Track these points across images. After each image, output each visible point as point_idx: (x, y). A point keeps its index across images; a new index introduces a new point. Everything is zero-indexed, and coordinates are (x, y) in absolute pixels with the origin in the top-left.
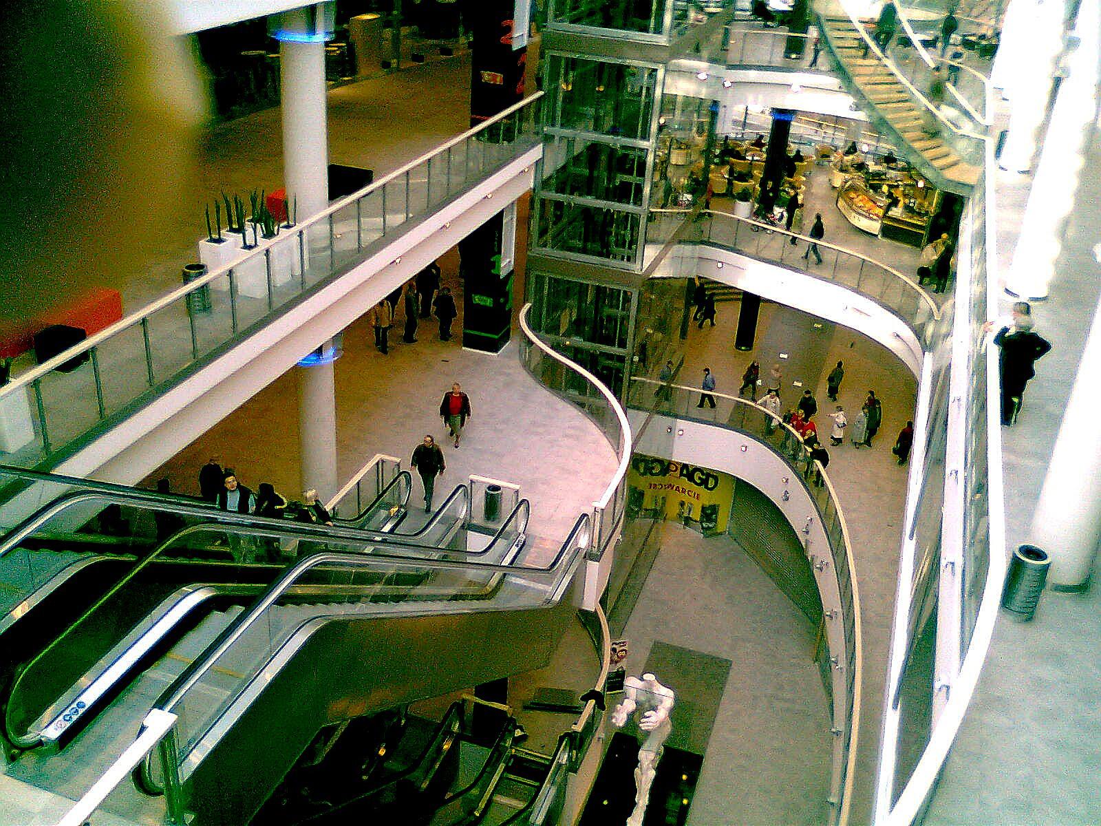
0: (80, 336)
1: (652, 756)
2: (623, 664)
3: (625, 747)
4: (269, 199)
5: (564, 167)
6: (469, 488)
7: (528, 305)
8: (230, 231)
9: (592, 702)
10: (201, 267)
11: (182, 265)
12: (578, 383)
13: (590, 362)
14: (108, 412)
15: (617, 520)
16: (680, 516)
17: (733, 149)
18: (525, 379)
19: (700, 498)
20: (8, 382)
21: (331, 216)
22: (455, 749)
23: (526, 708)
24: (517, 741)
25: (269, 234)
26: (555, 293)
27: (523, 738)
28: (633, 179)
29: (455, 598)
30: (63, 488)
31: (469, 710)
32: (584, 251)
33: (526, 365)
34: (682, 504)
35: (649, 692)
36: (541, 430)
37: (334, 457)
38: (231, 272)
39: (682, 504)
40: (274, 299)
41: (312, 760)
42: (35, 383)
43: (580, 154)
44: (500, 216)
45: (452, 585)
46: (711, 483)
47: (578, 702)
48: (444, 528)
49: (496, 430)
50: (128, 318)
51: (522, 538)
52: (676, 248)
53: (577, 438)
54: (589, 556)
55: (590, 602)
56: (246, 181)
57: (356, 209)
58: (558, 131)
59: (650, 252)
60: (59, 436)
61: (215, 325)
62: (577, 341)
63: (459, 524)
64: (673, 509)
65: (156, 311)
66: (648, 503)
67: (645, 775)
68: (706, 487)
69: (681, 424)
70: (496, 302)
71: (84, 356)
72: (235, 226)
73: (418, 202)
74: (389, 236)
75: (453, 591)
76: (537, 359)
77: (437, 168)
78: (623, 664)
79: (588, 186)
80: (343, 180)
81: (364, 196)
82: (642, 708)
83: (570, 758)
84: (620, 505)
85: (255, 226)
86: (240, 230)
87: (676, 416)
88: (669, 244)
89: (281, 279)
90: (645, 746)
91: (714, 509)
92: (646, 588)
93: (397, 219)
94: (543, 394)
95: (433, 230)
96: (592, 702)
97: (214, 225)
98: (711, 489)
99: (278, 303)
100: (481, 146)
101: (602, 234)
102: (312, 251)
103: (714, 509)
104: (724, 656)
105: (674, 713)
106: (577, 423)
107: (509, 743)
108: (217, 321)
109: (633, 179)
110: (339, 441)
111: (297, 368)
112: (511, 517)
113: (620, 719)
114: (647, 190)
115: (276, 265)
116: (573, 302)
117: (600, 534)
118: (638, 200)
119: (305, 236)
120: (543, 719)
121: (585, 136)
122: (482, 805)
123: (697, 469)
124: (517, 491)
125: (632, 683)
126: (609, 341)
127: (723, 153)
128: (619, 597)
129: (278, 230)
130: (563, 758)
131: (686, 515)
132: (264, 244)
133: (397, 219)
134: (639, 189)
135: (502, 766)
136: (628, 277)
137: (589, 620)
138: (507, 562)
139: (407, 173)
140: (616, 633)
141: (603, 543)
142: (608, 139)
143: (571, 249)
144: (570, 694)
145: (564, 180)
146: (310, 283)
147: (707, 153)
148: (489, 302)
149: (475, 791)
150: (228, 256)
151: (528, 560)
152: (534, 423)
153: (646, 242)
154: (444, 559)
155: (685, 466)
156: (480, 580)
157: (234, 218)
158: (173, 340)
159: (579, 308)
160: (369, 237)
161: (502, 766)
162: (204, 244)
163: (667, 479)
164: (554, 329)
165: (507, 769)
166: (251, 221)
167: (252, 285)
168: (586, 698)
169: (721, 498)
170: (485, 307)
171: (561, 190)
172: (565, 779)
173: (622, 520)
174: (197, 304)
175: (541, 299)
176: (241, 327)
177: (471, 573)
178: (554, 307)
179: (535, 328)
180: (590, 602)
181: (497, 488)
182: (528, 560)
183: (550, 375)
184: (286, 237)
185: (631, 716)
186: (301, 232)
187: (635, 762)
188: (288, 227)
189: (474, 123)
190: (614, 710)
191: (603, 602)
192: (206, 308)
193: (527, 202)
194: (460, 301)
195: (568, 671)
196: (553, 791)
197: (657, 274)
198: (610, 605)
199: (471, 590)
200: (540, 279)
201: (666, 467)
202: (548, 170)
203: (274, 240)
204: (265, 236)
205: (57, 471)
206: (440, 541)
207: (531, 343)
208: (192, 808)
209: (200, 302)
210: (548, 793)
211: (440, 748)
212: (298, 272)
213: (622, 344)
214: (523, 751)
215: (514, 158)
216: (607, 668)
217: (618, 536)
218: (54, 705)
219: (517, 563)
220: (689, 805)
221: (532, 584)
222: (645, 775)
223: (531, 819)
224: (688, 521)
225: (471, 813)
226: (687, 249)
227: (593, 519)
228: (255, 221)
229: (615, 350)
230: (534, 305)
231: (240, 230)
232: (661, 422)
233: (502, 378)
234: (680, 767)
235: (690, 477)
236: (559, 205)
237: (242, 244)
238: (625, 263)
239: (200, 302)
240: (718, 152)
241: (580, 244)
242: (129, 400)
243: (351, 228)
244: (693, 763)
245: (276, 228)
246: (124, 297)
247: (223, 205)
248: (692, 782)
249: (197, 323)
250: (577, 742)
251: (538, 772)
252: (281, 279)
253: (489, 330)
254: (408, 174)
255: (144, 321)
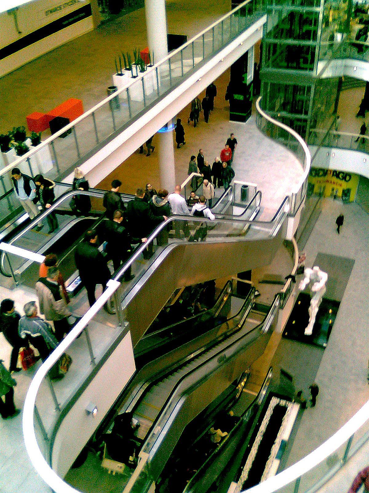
0: (67, 122)
1: (317, 302)
2: (304, 263)
3: (305, 299)
4: (142, 53)
5: (277, 26)
6: (234, 188)
7: (260, 98)
8: (125, 70)
9: (290, 280)
10: (114, 87)
11: (106, 87)
12: (284, 134)
13: (291, 124)
14: (82, 156)
15: (303, 197)
16: (332, 195)
17: (361, 9)
18: (258, 134)
19: (341, 186)
20: (40, 143)
21: (169, 59)
22: (229, 299)
23: (260, 282)
24: (256, 296)
25: (143, 70)
26: (273, 90)
27: (259, 295)
28: (312, 28)
29: (228, 236)
30: (66, 189)
31: (235, 284)
32: (288, 67)
33: (259, 127)
34: (333, 190)
35: (316, 274)
36: (266, 158)
37: (174, 175)
38: (127, 89)
39: (333, 190)
40: (147, 101)
41: (170, 303)
42: (52, 143)
43: (285, 18)
44: (246, 54)
45: (227, 230)
46: (348, 178)
47: (283, 280)
48: (223, 205)
49: (245, 160)
50: (73, 122)
51: (258, 208)
52: (333, 63)
53: (284, 161)
54: (290, 215)
55: (290, 235)
56: (131, 46)
57: (180, 56)
58: (274, 7)
59: (321, 65)
60: (64, 166)
61: (122, 115)
62: (284, 114)
63: (229, 203)
64: (328, 192)
65: (98, 109)
66: (316, 189)
67: (314, 310)
68: (345, 180)
69: (334, 151)
70: (245, 97)
71: (69, 131)
72: (128, 67)
73: (208, 50)
74: (195, 68)
75: (226, 233)
76: (264, 124)
77: (216, 31)
78: (304, 263)
79: (290, 34)
80: (174, 41)
81: (183, 49)
82: (312, 283)
83: (280, 304)
84: (305, 191)
85: (137, 66)
86: (130, 69)
87: (332, 147)
88: (329, 61)
89: (148, 92)
90: (314, 298)
91: (349, 191)
92: (314, 229)
93: (198, 60)
94: (267, 141)
95: (192, 84)
96: (290, 280)
97: (119, 68)
98: (347, 181)
99: (148, 103)
100: (237, 19)
101: (301, 57)
102: (162, 77)
103: (349, 191)
104: (351, 257)
105: (327, 284)
106: (283, 154)
107: (253, 297)
108: (124, 112)
109: (312, 28)
110: (176, 168)
111: (157, 134)
112: (253, 200)
113: (302, 286)
114: (319, 33)
115: (147, 86)
116: (282, 95)
117: (295, 205)
118: (315, 39)
119: (158, 70)
120: (268, 287)
121: (287, 8)
122: (242, 323)
123: (340, 172)
124: (256, 188)
125: (308, 272)
126: (300, 112)
127: (356, 12)
128: (302, 234)
129: (146, 68)
130: (277, 303)
131: (335, 194)
132: (141, 75)
133: (198, 60)
134: (315, 33)
135: (250, 307)
136: (310, 78)
137: (288, 244)
138: (251, 219)
139: (203, 35)
140: (301, 249)
141: (297, 207)
142: (300, 9)
143: (280, 67)
144: (280, 276)
145: (278, 32)
146: (162, 93)
147: (349, 12)
148: (241, 98)
149: (238, 317)
150: (126, 82)
151: (261, 218)
152: (263, 155)
153: (318, 60)
154: (224, 218)
155: (335, 171)
156: (239, 228)
157: (127, 64)
158: (105, 122)
159: (285, 97)
160: (186, 70)
161: (250, 307)
162: (115, 77)
163: (326, 178)
164: (272, 109)
165: (252, 308)
166: (134, 64)
167: (137, 95)
168: (287, 278)
169: (353, 185)
170: (239, 101)
171: (276, 37)
172: (278, 312)
173: (305, 199)
174: (114, 105)
175: (266, 94)
176: (133, 115)
177: (236, 225)
178: (272, 98)
179: (264, 109)
180: (290, 235)
181: (246, 186)
182: (261, 218)
183: (271, 132)
184: (150, 71)
185: (307, 286)
186: (157, 68)
187: (309, 304)
188: (150, 66)
189: (233, 7)
190: (299, 282)
191: (295, 236)
192: (118, 107)
193: (260, 46)
194: (234, 95)
195: (279, 267)
196: (272, 317)
197: (324, 76)
198: (298, 237)
199: (235, 232)
200: (266, 84)
201: (325, 172)
202: (270, 28)
203: (145, 72)
204: (141, 72)
205: (62, 182)
206: (221, 211)
207: (261, 116)
208: (127, 320)
209: (115, 104)
210: (270, 318)
211: (222, 300)
212: (156, 88)
213: (306, 113)
214: (259, 301)
215: (253, 23)
216: (297, 265)
217: (303, 205)
218: (69, 279)
219: (256, 219)
220: (333, 323)
221: (263, 229)
222: (314, 310)
223: (263, 328)
224: (335, 197)
225: (237, 326)
226: (339, 62)
227: (291, 198)
228: (137, 64)
229: (303, 116)
230: (263, 98)
231: (130, 69)
232: (324, 150)
233: (247, 135)
234: (330, 306)
235: (337, 176)
236: (275, 45)
237: (131, 76)
238: (308, 72)
239: (115, 104)
240: (353, 10)
241: (285, 64)
242: (90, 149)
243: (178, 66)
244: (336, 305)
245: (145, 67)
246: (83, 102)
247: (122, 58)
248: (335, 313)
249: (115, 114)
250: (283, 297)
251: (266, 310)
252: (148, 92)
253: (240, 111)
254: (181, 51)
255: (93, 114)
